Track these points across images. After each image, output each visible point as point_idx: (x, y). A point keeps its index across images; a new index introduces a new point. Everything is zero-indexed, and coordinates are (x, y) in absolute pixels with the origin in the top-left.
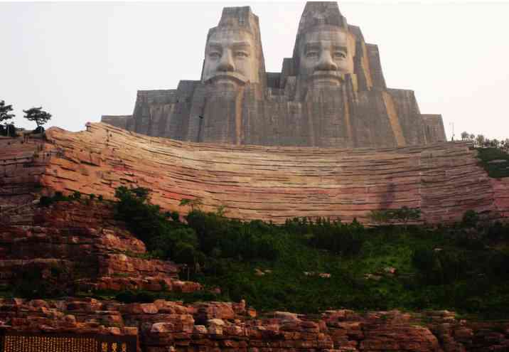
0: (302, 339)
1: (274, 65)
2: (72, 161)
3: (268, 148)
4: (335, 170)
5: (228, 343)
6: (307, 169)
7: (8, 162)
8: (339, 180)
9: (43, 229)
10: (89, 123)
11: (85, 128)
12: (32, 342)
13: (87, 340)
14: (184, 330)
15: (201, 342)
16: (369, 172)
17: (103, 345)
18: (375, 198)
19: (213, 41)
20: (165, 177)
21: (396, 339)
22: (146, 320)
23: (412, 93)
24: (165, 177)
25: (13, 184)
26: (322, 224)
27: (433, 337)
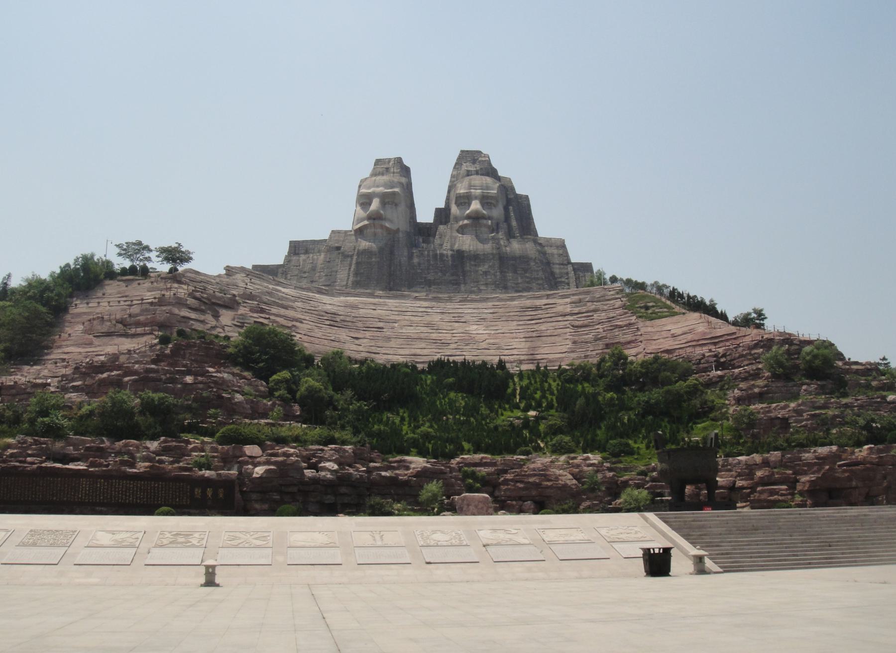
1: (425, 215)
3: (417, 295)
4: (484, 316)
5: (343, 490)
7: (135, 302)
8: (487, 327)
10: (228, 266)
11: (224, 272)
16: (516, 318)
17: (196, 490)
18: (523, 344)
19: (363, 191)
20: (304, 321)
22: (247, 463)
23: (462, 152)
24: (304, 321)
26: (507, 406)
27: (574, 482)
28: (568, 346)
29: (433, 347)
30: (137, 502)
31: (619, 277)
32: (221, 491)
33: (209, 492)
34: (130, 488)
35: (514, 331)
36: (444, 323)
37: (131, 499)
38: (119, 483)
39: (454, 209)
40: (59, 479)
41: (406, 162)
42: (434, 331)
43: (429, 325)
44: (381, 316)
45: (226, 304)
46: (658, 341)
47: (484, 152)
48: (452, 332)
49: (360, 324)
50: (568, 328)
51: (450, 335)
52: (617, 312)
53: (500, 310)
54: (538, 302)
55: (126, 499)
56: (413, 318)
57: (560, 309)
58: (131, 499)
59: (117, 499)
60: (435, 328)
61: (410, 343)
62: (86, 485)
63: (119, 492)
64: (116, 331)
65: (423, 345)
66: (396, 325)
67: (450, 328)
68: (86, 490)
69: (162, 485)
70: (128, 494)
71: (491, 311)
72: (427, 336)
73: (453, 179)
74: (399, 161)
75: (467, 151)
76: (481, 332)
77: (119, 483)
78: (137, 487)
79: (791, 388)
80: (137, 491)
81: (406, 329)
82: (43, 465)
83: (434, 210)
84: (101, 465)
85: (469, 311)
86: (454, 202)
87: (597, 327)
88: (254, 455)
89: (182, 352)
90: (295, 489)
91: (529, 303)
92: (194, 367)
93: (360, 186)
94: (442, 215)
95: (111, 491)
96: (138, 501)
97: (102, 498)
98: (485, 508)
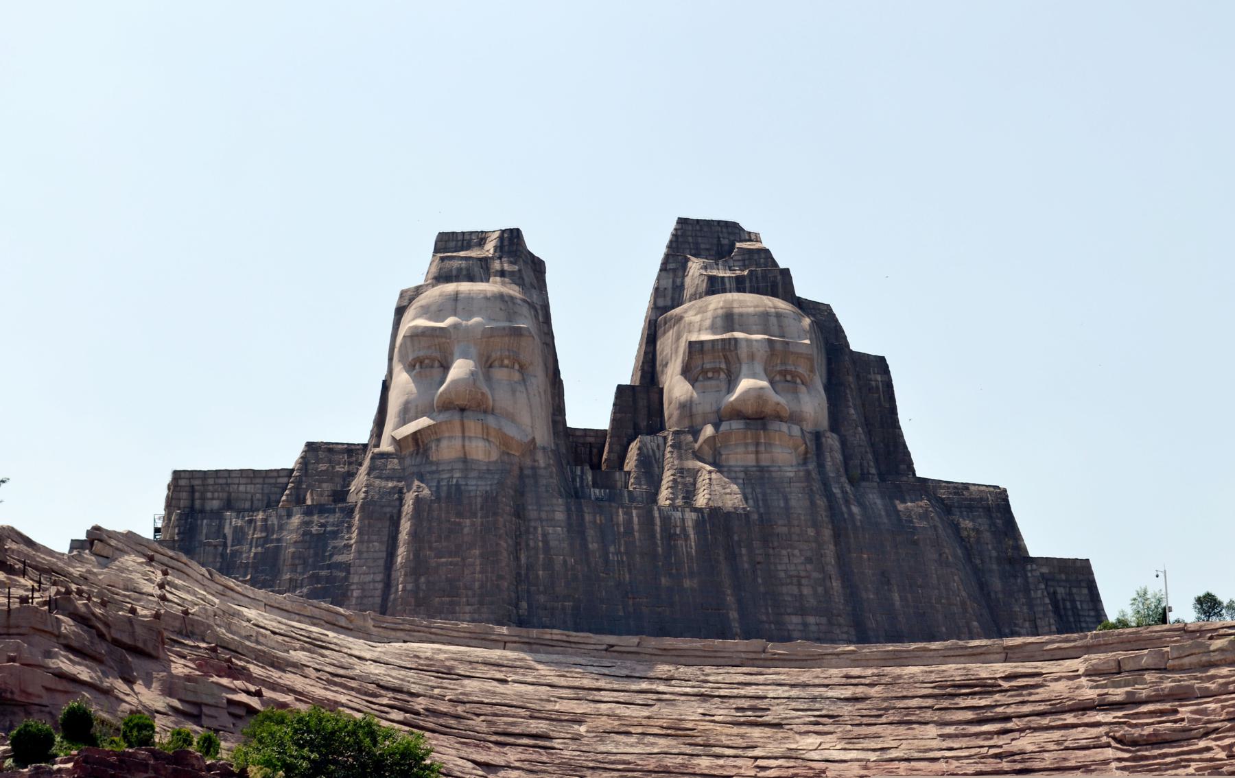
2: (92, 627)
4: (834, 709)
6: (745, 703)
9: (64, 663)
16: (936, 716)
31: (1224, 598)
36: (718, 728)
39: (676, 387)
41: (533, 244)
42: (698, 750)
43: (676, 730)
44: (529, 700)
45: (140, 645)
47: (747, 226)
48: (750, 753)
49: (478, 723)
50: (1108, 745)
51: (750, 762)
52: (990, 714)
53: (873, 691)
54: (984, 671)
56: (621, 710)
57: (1059, 689)
60: (699, 740)
66: (583, 729)
67: (739, 742)
71: (848, 692)
72: (683, 765)
73: (661, 303)
74: (512, 240)
75: (698, 221)
81: (617, 743)
83: (614, 389)
85: (781, 692)
87: (1202, 744)
91: (953, 670)
93: (400, 312)
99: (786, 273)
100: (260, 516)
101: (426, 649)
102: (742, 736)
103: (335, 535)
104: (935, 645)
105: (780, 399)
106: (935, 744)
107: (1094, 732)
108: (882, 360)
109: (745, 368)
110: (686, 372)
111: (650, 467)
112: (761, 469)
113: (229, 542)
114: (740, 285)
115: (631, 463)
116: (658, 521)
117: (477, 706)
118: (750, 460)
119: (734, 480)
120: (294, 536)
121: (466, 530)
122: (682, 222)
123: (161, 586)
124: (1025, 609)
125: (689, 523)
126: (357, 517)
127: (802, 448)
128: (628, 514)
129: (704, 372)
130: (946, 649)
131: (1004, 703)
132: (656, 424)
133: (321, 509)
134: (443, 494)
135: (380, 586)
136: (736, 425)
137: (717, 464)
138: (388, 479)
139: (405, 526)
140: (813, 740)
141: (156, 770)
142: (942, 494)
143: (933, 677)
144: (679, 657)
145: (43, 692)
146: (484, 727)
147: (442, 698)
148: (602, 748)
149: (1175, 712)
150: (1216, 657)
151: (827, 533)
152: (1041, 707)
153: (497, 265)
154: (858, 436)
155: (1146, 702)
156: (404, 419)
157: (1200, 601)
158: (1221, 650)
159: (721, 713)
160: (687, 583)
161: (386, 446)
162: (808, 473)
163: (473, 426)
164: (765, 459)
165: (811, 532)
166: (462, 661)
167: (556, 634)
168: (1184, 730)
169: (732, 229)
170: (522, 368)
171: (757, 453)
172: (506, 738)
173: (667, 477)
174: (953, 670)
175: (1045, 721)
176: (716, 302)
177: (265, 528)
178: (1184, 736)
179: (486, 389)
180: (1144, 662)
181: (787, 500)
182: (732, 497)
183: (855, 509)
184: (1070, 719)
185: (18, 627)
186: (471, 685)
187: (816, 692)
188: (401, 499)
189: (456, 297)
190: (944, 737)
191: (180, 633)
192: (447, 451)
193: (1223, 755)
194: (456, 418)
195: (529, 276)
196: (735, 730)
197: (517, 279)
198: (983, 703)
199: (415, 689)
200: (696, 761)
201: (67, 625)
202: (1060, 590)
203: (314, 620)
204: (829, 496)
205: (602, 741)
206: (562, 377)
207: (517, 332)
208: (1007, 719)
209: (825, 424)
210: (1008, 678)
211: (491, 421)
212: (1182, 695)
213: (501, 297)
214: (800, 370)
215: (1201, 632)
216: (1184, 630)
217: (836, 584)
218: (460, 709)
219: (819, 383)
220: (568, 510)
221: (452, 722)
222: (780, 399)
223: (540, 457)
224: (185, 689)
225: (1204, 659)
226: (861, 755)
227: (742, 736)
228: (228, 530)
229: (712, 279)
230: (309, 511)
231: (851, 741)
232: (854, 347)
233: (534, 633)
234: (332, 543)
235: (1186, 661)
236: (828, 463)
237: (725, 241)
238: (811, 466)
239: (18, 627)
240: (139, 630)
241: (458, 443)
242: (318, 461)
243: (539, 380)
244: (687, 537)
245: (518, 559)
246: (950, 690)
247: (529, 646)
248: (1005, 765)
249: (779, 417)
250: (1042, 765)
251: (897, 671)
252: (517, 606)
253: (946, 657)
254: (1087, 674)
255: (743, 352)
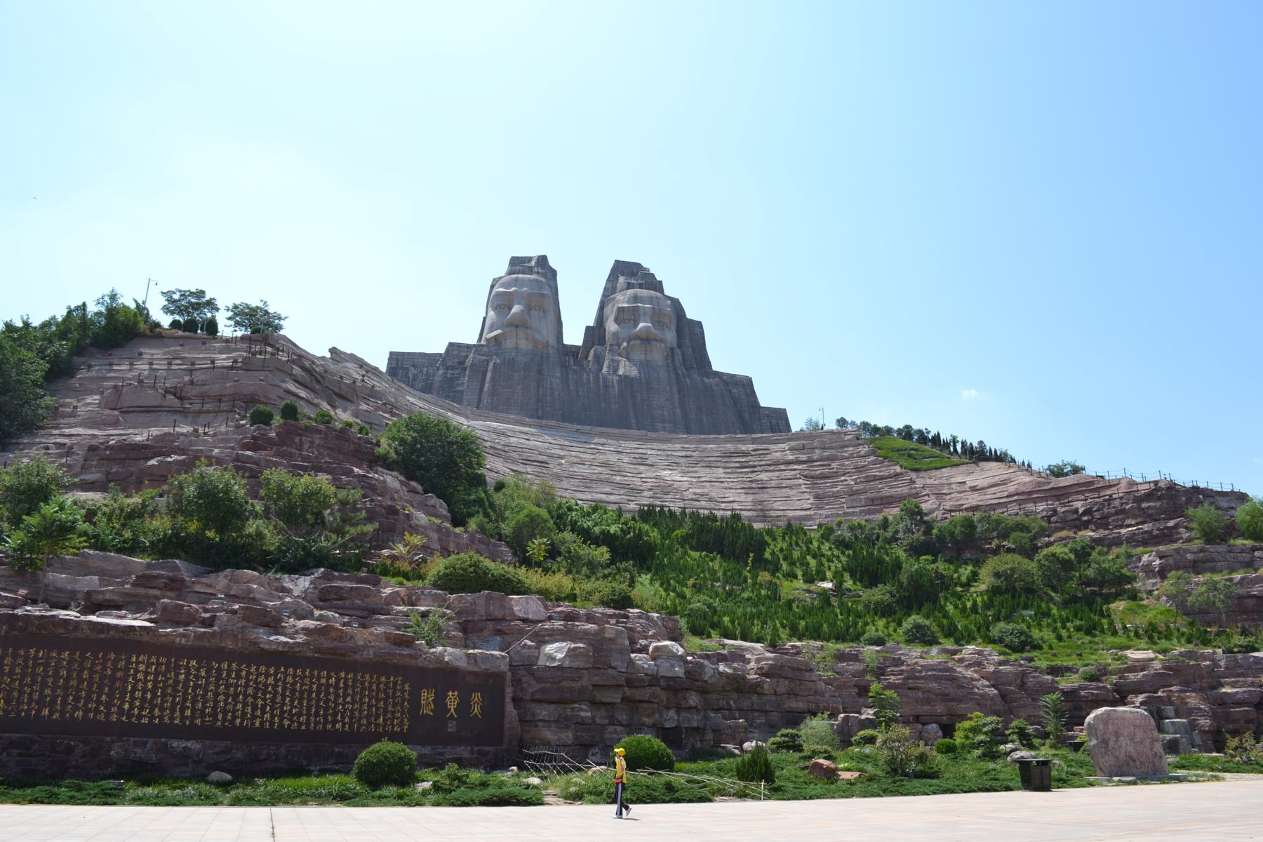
0: (792, 693)
1: (573, 336)
2: (313, 375)
4: (677, 460)
6: (637, 456)
9: (291, 386)
10: (334, 348)
11: (328, 355)
12: (219, 677)
13: (383, 679)
14: (614, 664)
15: (646, 693)
16: (723, 465)
17: (424, 694)
21: (937, 695)
25: (204, 397)
28: (809, 501)
29: (621, 492)
30: (281, 725)
31: (849, 419)
32: (476, 697)
33: (452, 701)
34: (266, 685)
35: (724, 480)
37: (267, 716)
38: (239, 671)
39: (611, 326)
40: (66, 655)
41: (552, 263)
42: (616, 473)
43: (606, 465)
45: (343, 393)
46: (952, 495)
49: (515, 455)
51: (639, 480)
53: (694, 454)
54: (743, 448)
55: (254, 717)
56: (581, 455)
58: (267, 716)
59: (229, 716)
60: (616, 469)
61: (589, 485)
62: (146, 674)
63: (236, 696)
64: (165, 404)
65: (607, 489)
66: (563, 461)
68: (145, 691)
69: (346, 679)
70: (260, 702)
71: (683, 454)
73: (606, 294)
74: (543, 260)
76: (677, 478)
77: (239, 671)
78: (285, 683)
79: (1239, 555)
80: (284, 696)
82: (19, 612)
83: (584, 328)
84: (190, 620)
85: (653, 452)
86: (612, 318)
87: (843, 478)
88: (530, 617)
89: (297, 439)
90: (616, 698)
91: (730, 447)
92: (325, 462)
93: (492, 287)
94: (595, 334)
95: (216, 694)
96: (286, 723)
97: (188, 712)
98: (1148, 741)
99: (660, 282)
100: (425, 369)
101: (494, 425)
102: (636, 469)
103: (457, 379)
104: (722, 436)
105: (656, 332)
106: (722, 476)
107: (793, 473)
108: (700, 322)
109: (642, 319)
110: (616, 320)
111: (599, 359)
112: (648, 361)
113: (411, 380)
114: (641, 286)
115: (591, 357)
116: (601, 380)
117: (514, 448)
118: (643, 357)
119: (635, 365)
120: (440, 379)
121: (516, 378)
122: (617, 262)
123: (363, 376)
124: (759, 427)
125: (615, 381)
126: (468, 371)
127: (665, 354)
128: (588, 375)
129: (624, 320)
130: (727, 438)
131: (753, 460)
132: (602, 341)
133: (452, 368)
134: (506, 362)
135: (476, 401)
136: (637, 342)
137: (628, 359)
138: (484, 355)
139: (489, 375)
140: (667, 472)
141: (326, 434)
142: (725, 378)
143: (721, 449)
144: (608, 436)
145: (277, 399)
146: (517, 457)
147: (499, 443)
148: (571, 469)
149: (830, 465)
150: (847, 443)
151: (675, 389)
152: (769, 463)
153: (536, 270)
154: (689, 352)
155: (816, 461)
156: (491, 330)
157: (838, 421)
158: (850, 440)
159: (626, 459)
160: (613, 406)
161: (483, 342)
162: (668, 363)
163: (521, 332)
164: (649, 357)
165: (668, 388)
166: (510, 430)
167: (554, 423)
168: (834, 472)
169: (638, 266)
170: (544, 311)
171: (646, 354)
172: (527, 462)
173: (606, 363)
174: (730, 447)
175: (772, 468)
176: (630, 292)
177: (427, 374)
178: (835, 475)
179: (527, 318)
180: (815, 445)
181: (658, 374)
182: (634, 372)
183: (687, 380)
184: (782, 467)
185: (268, 367)
186: (512, 440)
187: (669, 453)
188: (488, 364)
189: (517, 279)
190: (726, 473)
191: (369, 396)
192: (509, 344)
193: (853, 483)
194: (514, 329)
195: (549, 275)
196: (633, 466)
197: (544, 275)
198: (743, 460)
199: (486, 438)
200: (614, 477)
201: (297, 370)
202: (773, 421)
203: (441, 407)
204: (677, 374)
205: (572, 467)
206: (562, 319)
207: (543, 295)
208: (755, 466)
209: (675, 345)
210: (754, 450)
211: (529, 332)
212: (832, 459)
213: (536, 281)
214: (666, 321)
215: (839, 433)
216: (832, 432)
217: (678, 411)
218: (506, 449)
219: (673, 328)
220: (562, 373)
221: (503, 453)
222: (656, 332)
223: (550, 349)
224: (364, 415)
225: (842, 444)
226: (689, 479)
227: (636, 469)
228: (410, 375)
229: (629, 284)
230: (447, 368)
231: (684, 473)
232: (688, 317)
233: (544, 422)
234: (456, 382)
235: (834, 444)
236: (677, 362)
237: (635, 271)
238: (669, 361)
239: (268, 367)
240: (343, 386)
241: (514, 340)
242: (453, 350)
243: (551, 317)
244: (614, 387)
245: (538, 391)
246: (731, 454)
247: (541, 427)
248: (754, 485)
249: (656, 340)
250: (772, 485)
251: (705, 446)
252: (537, 412)
253: (727, 441)
254: (789, 450)
255: (641, 312)
